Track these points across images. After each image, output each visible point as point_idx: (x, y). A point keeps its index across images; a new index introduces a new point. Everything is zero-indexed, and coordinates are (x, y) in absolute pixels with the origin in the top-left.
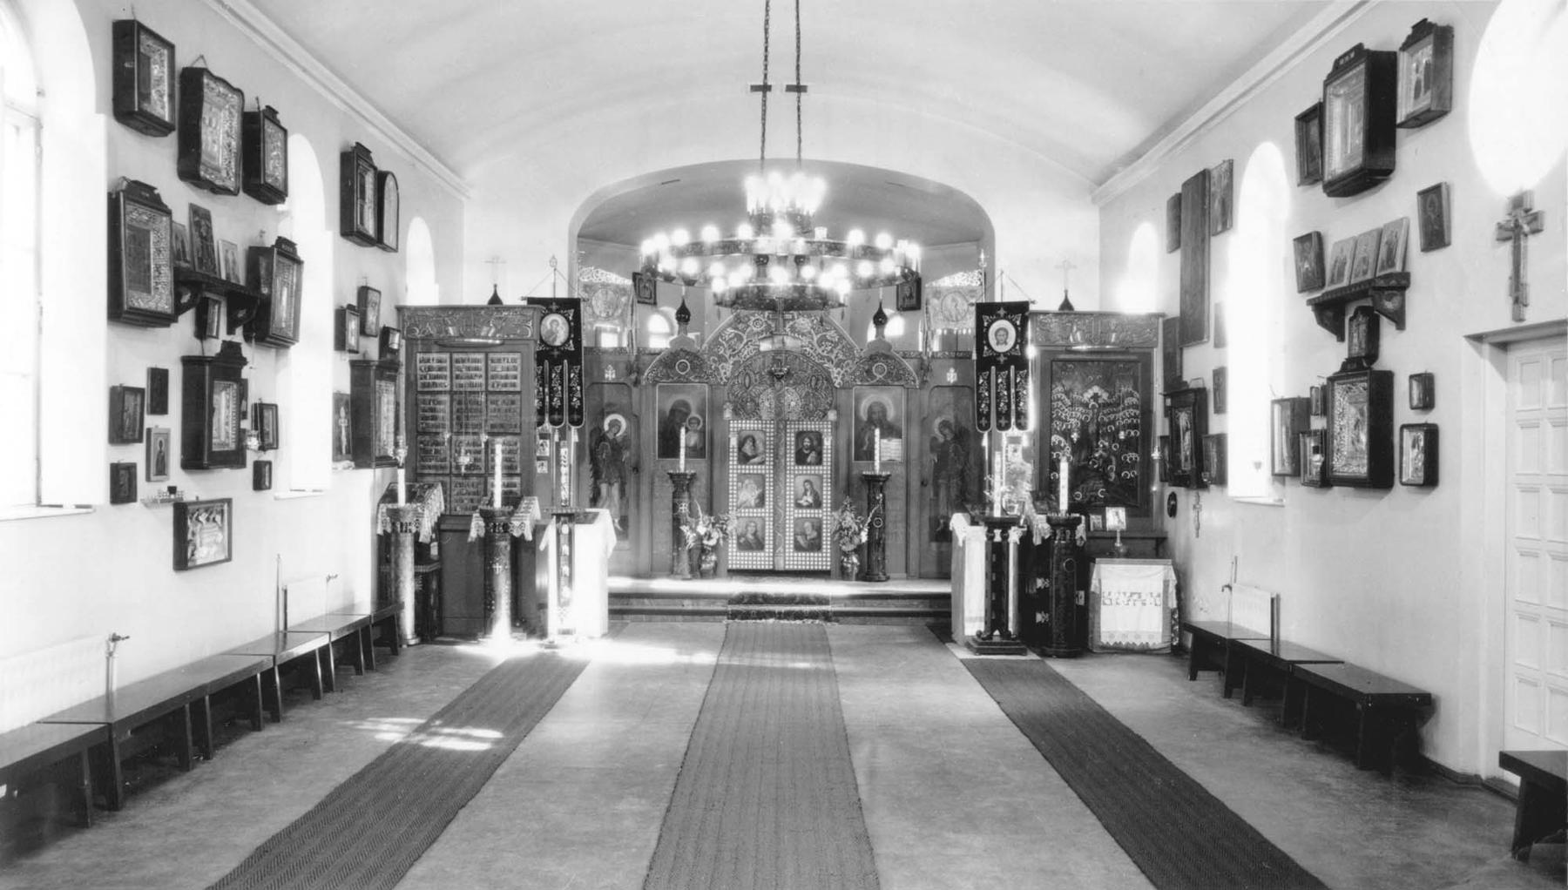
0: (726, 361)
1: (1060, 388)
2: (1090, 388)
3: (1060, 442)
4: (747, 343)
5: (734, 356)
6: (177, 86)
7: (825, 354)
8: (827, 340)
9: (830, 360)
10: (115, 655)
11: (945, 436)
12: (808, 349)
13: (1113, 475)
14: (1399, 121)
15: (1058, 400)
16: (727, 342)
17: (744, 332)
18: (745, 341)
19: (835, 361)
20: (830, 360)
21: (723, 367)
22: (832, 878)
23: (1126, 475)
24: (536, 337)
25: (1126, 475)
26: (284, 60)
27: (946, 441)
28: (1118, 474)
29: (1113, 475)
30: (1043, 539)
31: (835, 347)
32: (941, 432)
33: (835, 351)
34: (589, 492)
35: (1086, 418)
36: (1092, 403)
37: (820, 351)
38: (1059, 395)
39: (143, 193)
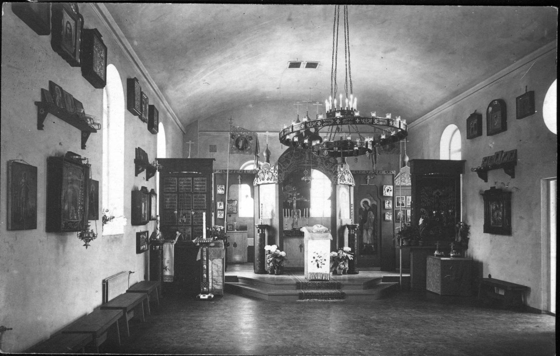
32: (364, 206)
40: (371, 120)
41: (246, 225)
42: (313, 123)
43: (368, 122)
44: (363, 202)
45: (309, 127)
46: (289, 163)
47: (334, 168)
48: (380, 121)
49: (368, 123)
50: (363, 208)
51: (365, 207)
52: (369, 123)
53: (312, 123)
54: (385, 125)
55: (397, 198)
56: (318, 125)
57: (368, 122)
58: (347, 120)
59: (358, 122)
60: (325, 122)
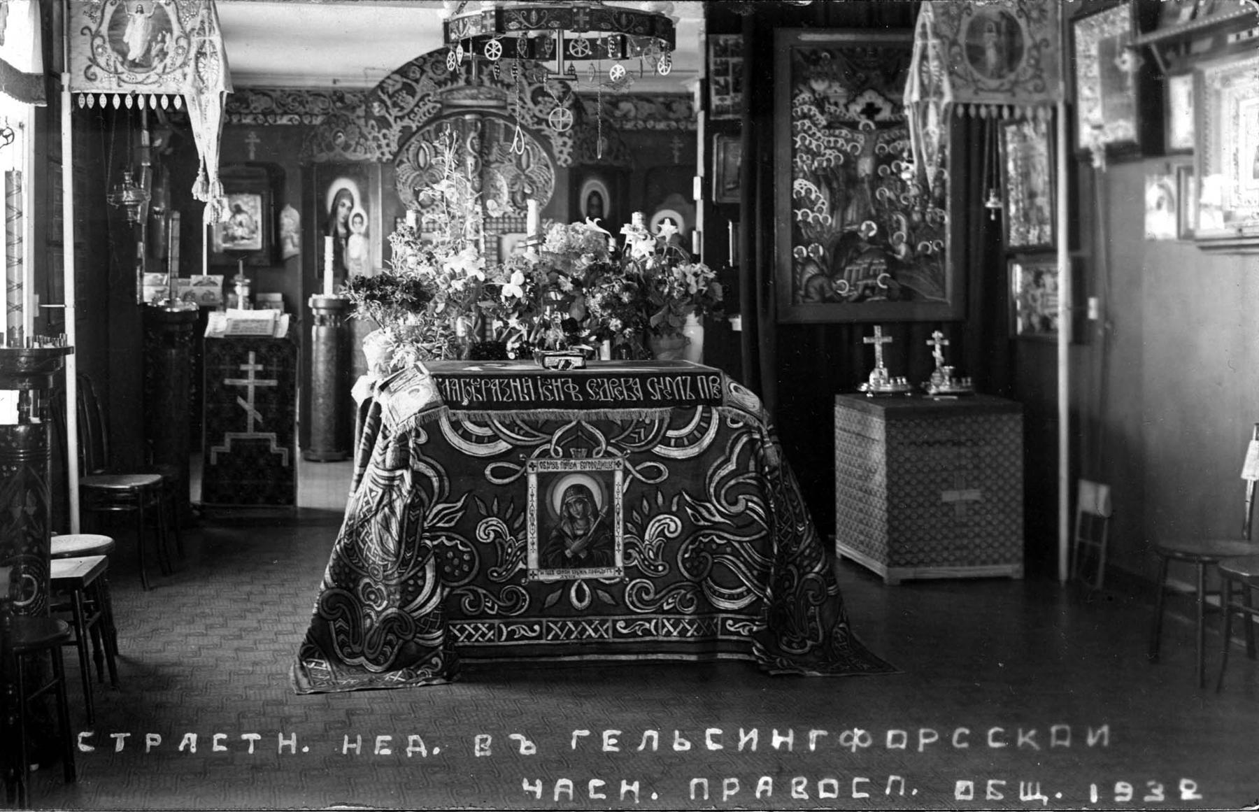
0: (389, 126)
1: (806, 95)
2: (861, 95)
3: (809, 191)
5: (402, 118)
6: (138, 288)
13: (903, 249)
15: (805, 116)
16: (390, 97)
21: (385, 136)
23: (926, 247)
25: (926, 247)
26: (1075, 553)
28: (911, 246)
29: (903, 249)
30: (630, 222)
34: (365, 349)
35: (854, 147)
36: (864, 121)
38: (806, 108)
39: (51, 385)
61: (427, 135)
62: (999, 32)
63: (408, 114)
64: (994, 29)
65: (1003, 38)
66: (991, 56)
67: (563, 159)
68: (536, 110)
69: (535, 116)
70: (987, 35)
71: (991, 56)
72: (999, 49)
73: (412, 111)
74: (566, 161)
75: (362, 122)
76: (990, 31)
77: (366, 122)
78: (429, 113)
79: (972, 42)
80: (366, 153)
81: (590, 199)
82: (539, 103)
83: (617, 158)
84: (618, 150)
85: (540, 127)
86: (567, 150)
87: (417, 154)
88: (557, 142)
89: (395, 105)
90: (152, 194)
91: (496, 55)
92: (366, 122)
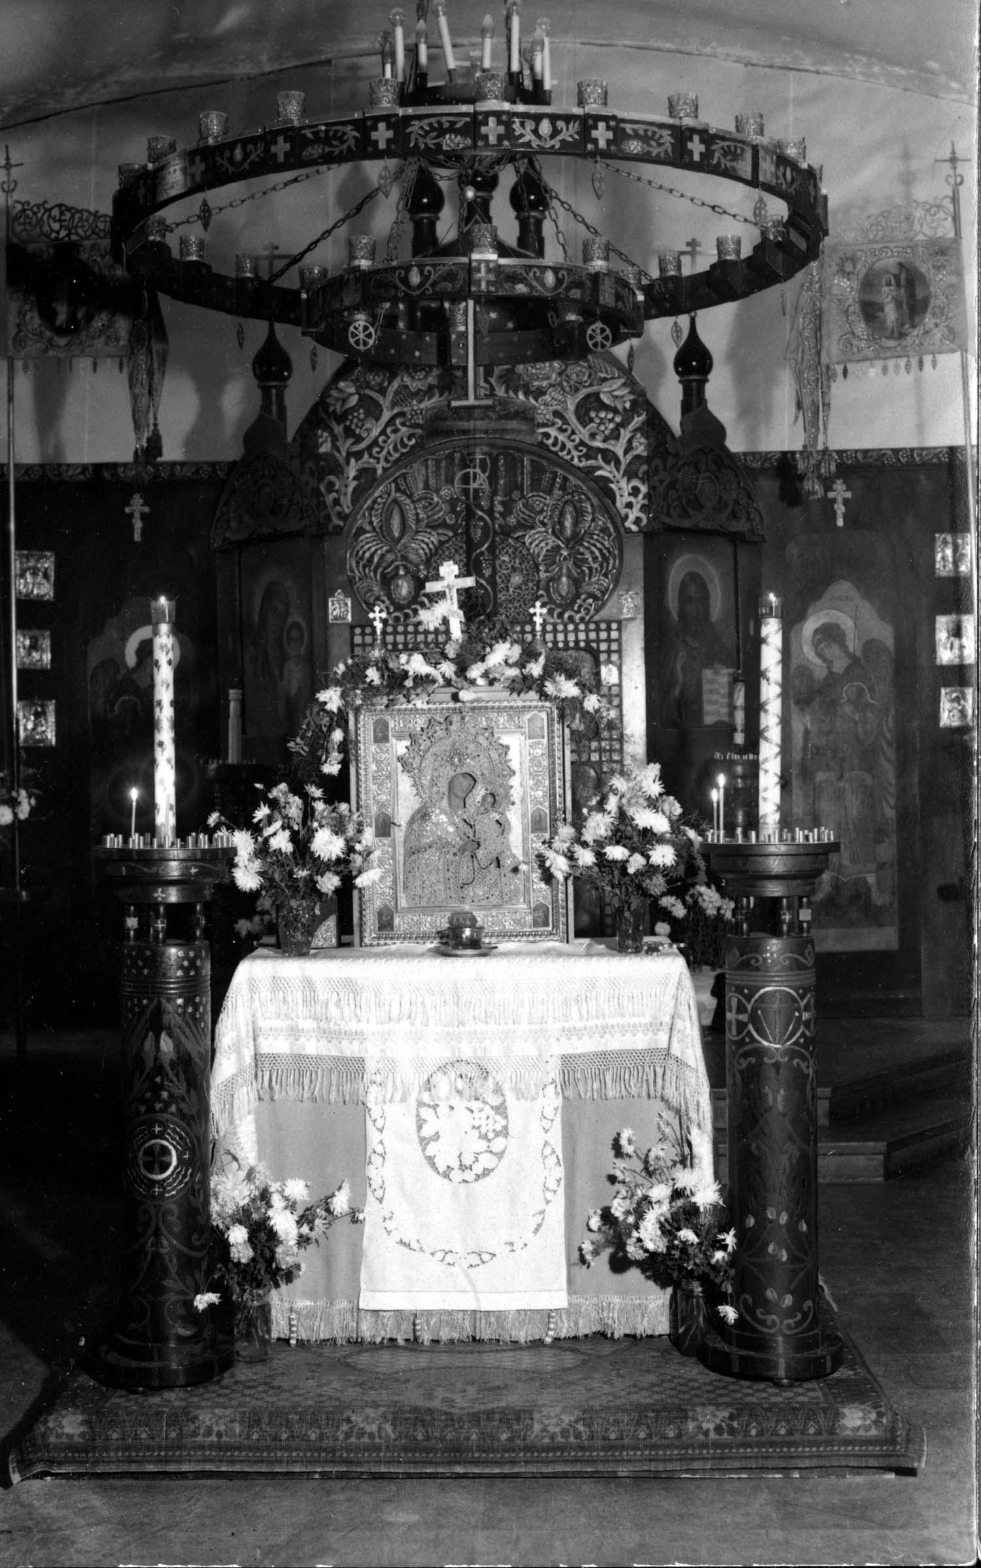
4: (391, 421)
7: (597, 443)
8: (604, 407)
9: (610, 457)
10: (793, 410)
11: (828, 662)
12: (553, 432)
14: (278, 326)
17: (383, 391)
18: (386, 416)
19: (625, 461)
20: (610, 457)
22: (505, 891)
24: (502, 73)
27: (831, 674)
31: (624, 424)
32: (820, 655)
33: (625, 434)
37: (583, 433)
40: (574, 127)
41: (952, 450)
42: (250, 147)
43: (552, 137)
44: (816, 631)
45: (231, 169)
46: (377, 419)
47: (630, 441)
48: (629, 137)
49: (556, 143)
50: (817, 661)
51: (825, 660)
52: (563, 142)
53: (244, 148)
54: (657, 161)
55: (547, 925)
56: (595, 142)
57: (552, 137)
58: (433, 129)
59: (281, 158)
60: (311, 142)
61: (401, 482)
62: (898, 285)
63: (369, 448)
64: (893, 282)
65: (903, 291)
66: (890, 314)
67: (632, 517)
68: (583, 433)
69: (582, 443)
70: (885, 289)
71: (890, 314)
72: (899, 305)
73: (375, 443)
74: (637, 521)
75: (296, 464)
76: (889, 284)
77: (303, 464)
78: (404, 445)
79: (867, 298)
80: (302, 518)
81: (683, 587)
82: (591, 420)
83: (734, 516)
84: (737, 502)
85: (591, 462)
86: (639, 501)
87: (389, 517)
88: (623, 488)
89: (349, 432)
90: (187, 1080)
91: (365, 343)
92: (303, 464)
